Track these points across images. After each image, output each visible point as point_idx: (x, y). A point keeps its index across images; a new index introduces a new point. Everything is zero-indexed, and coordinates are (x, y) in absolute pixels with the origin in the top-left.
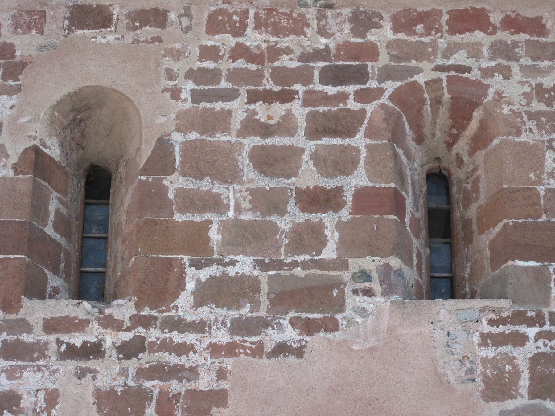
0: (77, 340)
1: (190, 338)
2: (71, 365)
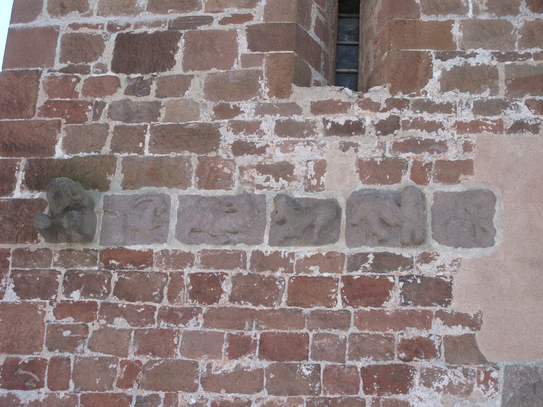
0: (341, 119)
1: (439, 117)
2: (336, 140)
